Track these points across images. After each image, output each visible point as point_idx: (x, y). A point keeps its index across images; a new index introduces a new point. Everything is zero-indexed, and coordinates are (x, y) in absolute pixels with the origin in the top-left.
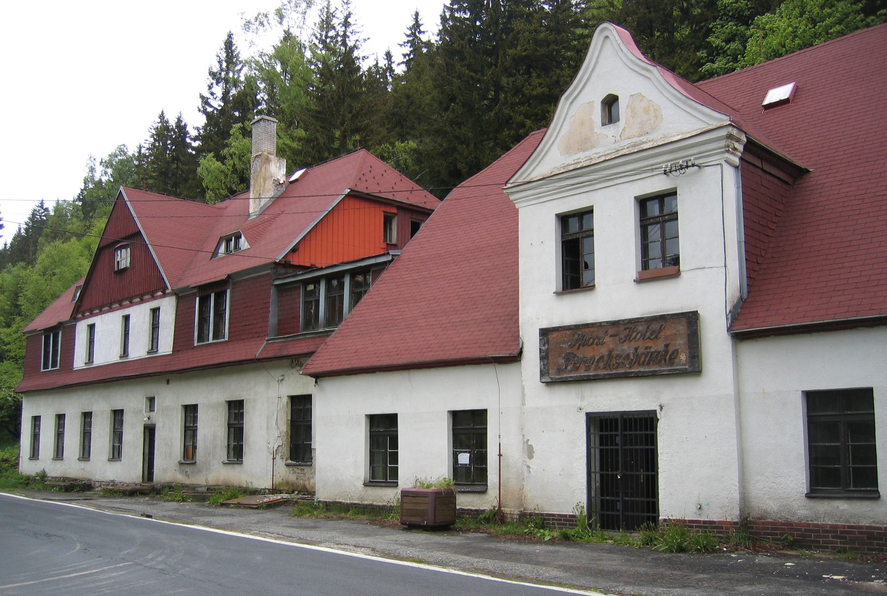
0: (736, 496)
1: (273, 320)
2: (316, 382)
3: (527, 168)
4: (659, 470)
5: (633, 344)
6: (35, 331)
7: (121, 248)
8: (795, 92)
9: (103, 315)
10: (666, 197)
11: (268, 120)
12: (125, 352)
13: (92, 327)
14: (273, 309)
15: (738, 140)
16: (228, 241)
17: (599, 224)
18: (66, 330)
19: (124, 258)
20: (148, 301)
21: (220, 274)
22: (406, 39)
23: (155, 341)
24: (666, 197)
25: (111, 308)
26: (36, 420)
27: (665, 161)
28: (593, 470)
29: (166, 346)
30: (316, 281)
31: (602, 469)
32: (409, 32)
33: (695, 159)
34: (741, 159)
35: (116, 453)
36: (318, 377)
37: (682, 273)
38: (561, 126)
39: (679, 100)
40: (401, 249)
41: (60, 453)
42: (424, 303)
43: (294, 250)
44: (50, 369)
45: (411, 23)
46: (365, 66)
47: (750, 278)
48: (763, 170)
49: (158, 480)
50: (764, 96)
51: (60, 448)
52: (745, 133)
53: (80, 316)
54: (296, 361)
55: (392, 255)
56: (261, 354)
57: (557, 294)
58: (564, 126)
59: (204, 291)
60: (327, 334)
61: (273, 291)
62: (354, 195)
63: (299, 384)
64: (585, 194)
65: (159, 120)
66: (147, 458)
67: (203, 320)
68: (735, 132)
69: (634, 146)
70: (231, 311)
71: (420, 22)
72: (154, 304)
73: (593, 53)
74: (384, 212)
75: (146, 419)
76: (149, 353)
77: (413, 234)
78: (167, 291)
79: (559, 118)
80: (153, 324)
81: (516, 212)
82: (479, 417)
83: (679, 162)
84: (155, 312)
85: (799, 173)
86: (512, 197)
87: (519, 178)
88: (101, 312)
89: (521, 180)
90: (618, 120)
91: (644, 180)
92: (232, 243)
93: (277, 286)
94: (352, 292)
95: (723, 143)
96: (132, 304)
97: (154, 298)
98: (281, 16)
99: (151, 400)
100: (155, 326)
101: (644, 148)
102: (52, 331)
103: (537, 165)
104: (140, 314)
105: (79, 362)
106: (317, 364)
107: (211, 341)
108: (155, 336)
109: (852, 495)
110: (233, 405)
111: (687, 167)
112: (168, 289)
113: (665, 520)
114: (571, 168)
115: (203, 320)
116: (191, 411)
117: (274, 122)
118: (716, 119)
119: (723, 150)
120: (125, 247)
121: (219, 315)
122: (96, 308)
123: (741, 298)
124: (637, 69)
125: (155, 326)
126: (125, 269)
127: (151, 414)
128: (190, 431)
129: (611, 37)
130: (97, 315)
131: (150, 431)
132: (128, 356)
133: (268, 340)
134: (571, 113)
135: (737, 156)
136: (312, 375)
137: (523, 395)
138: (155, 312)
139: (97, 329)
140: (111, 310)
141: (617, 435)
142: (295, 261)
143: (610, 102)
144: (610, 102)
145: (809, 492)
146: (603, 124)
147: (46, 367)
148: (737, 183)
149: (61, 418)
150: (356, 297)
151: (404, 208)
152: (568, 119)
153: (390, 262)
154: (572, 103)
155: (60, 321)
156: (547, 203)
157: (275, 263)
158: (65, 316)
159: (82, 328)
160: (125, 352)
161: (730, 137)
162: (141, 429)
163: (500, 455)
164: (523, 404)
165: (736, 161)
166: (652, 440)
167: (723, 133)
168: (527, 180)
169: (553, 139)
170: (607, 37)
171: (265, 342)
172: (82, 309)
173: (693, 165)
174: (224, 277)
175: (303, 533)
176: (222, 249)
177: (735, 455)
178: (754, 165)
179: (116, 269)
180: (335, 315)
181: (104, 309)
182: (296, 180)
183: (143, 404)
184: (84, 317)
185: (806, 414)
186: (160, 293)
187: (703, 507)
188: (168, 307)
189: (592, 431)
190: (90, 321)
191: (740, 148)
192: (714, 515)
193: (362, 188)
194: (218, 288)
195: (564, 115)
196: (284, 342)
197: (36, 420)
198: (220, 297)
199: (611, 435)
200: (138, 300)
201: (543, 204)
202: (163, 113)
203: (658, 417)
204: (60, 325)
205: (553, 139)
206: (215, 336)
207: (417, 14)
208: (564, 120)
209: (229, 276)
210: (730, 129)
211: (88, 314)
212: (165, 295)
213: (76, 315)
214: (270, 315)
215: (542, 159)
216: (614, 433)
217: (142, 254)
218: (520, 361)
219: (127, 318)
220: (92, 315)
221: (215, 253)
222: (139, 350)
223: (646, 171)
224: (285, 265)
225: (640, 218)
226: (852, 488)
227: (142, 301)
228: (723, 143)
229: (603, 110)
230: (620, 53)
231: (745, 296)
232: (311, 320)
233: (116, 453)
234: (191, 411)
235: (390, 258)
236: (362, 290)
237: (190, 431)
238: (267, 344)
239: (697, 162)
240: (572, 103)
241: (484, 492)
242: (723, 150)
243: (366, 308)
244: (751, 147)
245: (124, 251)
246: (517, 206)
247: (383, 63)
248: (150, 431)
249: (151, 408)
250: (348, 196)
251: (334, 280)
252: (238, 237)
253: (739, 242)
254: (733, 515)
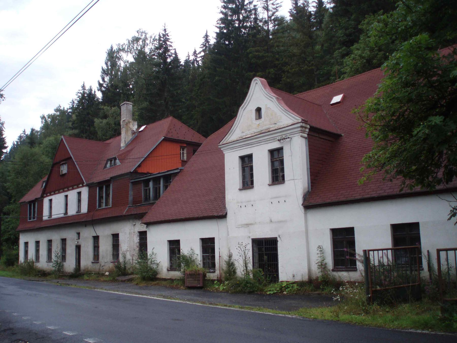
0: (306, 270)
1: (130, 198)
2: (147, 227)
3: (227, 137)
4: (279, 261)
6: (25, 202)
7: (63, 164)
8: (343, 99)
9: (56, 195)
10: (280, 150)
11: (128, 104)
12: (66, 213)
13: (51, 200)
14: (131, 193)
15: (306, 128)
16: (111, 161)
18: (40, 201)
19: (64, 169)
20: (76, 189)
21: (108, 177)
23: (80, 207)
24: (280, 150)
25: (59, 192)
26: (26, 244)
27: (279, 137)
28: (255, 262)
29: (84, 209)
30: (148, 181)
31: (259, 261)
33: (289, 135)
34: (308, 134)
36: (148, 224)
37: (286, 182)
38: (240, 120)
39: (283, 110)
40: (184, 166)
41: (38, 259)
42: (191, 192)
43: (139, 166)
44: (32, 220)
46: (182, 59)
47: (313, 183)
48: (319, 137)
50: (331, 99)
51: (38, 257)
52: (309, 124)
53: (45, 195)
54: (139, 217)
55: (180, 169)
56: (125, 213)
57: (240, 190)
58: (241, 120)
59: (101, 184)
60: (153, 204)
61: (130, 185)
62: (166, 140)
63: (140, 227)
64: (249, 148)
66: (77, 261)
67: (101, 197)
68: (304, 125)
69: (267, 129)
70: (113, 193)
72: (78, 190)
73: (251, 92)
74: (180, 146)
75: (76, 243)
76: (77, 212)
77: (193, 154)
78: (84, 184)
79: (239, 116)
80: (78, 199)
81: (223, 156)
82: (212, 240)
83: (283, 137)
84: (79, 193)
85: (337, 137)
86: (222, 149)
87: (224, 141)
88: (55, 194)
89: (224, 143)
90: (261, 118)
91: (271, 143)
92: (113, 162)
93: (131, 182)
94: (164, 186)
95: (299, 129)
96: (68, 190)
97: (78, 187)
99: (79, 234)
100: (79, 201)
101: (271, 130)
102: (32, 202)
103: (231, 135)
104: (72, 194)
106: (147, 218)
107: (104, 207)
108: (80, 205)
109: (349, 269)
110: (246, 159)
111: (286, 138)
112: (84, 183)
114: (244, 137)
115: (101, 197)
116: (96, 239)
117: (131, 104)
118: (296, 119)
119: (299, 132)
120: (65, 164)
121: (108, 195)
122: (52, 192)
123: (308, 191)
124: (268, 97)
125: (79, 201)
126: (65, 174)
127: (78, 240)
128: (96, 247)
129: (258, 83)
130: (53, 195)
131: (78, 248)
132: (67, 214)
133: (129, 207)
134: (244, 114)
135: (306, 134)
136: (145, 224)
137: (228, 232)
138: (79, 193)
139: (53, 202)
140: (59, 193)
141: (263, 248)
142: (140, 171)
143: (259, 110)
144: (259, 110)
145: (333, 268)
146: (256, 119)
148: (306, 144)
149: (38, 243)
150: (166, 187)
151: (189, 144)
152: (243, 117)
153: (179, 172)
154: (244, 110)
155: (36, 198)
156: (235, 152)
157: (131, 172)
158: (39, 196)
159: (46, 201)
160: (66, 213)
161: (302, 127)
162: (74, 247)
163: (220, 257)
164: (228, 235)
165: (306, 135)
166: (276, 249)
167: (299, 125)
169: (237, 125)
170: (257, 83)
171: (127, 208)
172: (46, 192)
173: (288, 138)
174: (109, 178)
175: (139, 291)
176: (108, 165)
177: (306, 255)
178: (314, 136)
179: (61, 174)
180: (157, 196)
181: (56, 192)
182: (142, 131)
183: (76, 236)
184: (47, 196)
185: (332, 238)
186: (81, 185)
187: (295, 276)
188: (85, 191)
189: (254, 246)
190: (50, 198)
191: (307, 130)
192: (298, 278)
193: (169, 136)
194: (107, 183)
195: (241, 114)
196: (135, 208)
197: (26, 244)
198: (108, 187)
199: (261, 248)
200: (71, 188)
201: (234, 152)
203: (278, 240)
204: (36, 199)
205: (237, 125)
206: (106, 205)
208: (241, 117)
209: (111, 178)
210: (301, 124)
211: (49, 194)
212: (83, 186)
214: (129, 195)
215: (234, 132)
216: (262, 247)
217: (72, 167)
218: (226, 217)
219: (66, 196)
220: (51, 195)
221: (105, 167)
222: (72, 211)
223: (269, 140)
224: (135, 172)
225: (271, 158)
226: (349, 267)
227: (73, 189)
228: (299, 129)
229: (256, 113)
230: (262, 90)
231: (310, 190)
232: (147, 198)
234: (96, 239)
235: (179, 171)
236: (168, 184)
237: (96, 247)
238: (128, 209)
239: (290, 136)
240: (244, 110)
241: (214, 272)
242: (299, 132)
243: (168, 193)
244: (312, 129)
246: (224, 153)
247: (192, 58)
248: (78, 248)
249: (79, 238)
250: (164, 139)
251: (156, 180)
252: (115, 159)
253: (307, 169)
254: (306, 278)
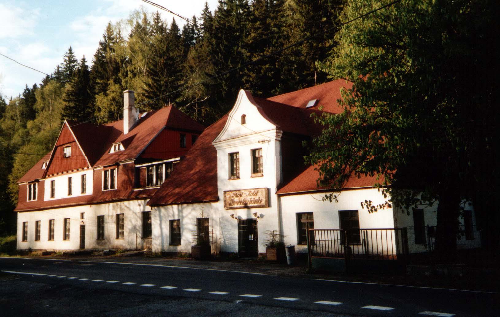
5: (250, 197)
13: (52, 182)
17: (240, 156)
22: (202, 16)
32: (203, 13)
35: (66, 237)
45: (204, 8)
49: (87, 248)
65: (69, 52)
71: (208, 7)
72: (83, 173)
98: (135, 65)
104: (76, 177)
105: (47, 197)
113: (260, 253)
143: (244, 117)
144: (244, 117)
147: (30, 199)
168: (219, 141)
202: (71, 48)
207: (207, 3)
213: (45, 175)
219: (70, 179)
222: (77, 192)
233: (66, 237)
245: (68, 148)
248: (83, 228)
